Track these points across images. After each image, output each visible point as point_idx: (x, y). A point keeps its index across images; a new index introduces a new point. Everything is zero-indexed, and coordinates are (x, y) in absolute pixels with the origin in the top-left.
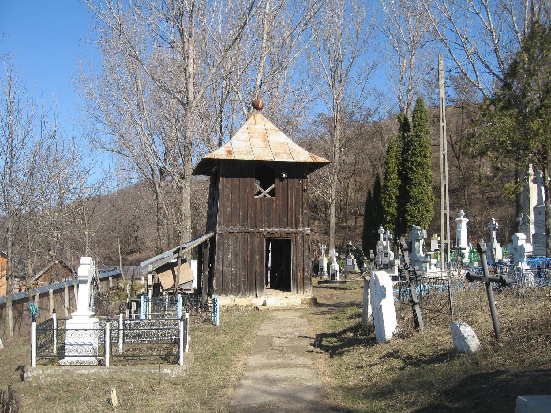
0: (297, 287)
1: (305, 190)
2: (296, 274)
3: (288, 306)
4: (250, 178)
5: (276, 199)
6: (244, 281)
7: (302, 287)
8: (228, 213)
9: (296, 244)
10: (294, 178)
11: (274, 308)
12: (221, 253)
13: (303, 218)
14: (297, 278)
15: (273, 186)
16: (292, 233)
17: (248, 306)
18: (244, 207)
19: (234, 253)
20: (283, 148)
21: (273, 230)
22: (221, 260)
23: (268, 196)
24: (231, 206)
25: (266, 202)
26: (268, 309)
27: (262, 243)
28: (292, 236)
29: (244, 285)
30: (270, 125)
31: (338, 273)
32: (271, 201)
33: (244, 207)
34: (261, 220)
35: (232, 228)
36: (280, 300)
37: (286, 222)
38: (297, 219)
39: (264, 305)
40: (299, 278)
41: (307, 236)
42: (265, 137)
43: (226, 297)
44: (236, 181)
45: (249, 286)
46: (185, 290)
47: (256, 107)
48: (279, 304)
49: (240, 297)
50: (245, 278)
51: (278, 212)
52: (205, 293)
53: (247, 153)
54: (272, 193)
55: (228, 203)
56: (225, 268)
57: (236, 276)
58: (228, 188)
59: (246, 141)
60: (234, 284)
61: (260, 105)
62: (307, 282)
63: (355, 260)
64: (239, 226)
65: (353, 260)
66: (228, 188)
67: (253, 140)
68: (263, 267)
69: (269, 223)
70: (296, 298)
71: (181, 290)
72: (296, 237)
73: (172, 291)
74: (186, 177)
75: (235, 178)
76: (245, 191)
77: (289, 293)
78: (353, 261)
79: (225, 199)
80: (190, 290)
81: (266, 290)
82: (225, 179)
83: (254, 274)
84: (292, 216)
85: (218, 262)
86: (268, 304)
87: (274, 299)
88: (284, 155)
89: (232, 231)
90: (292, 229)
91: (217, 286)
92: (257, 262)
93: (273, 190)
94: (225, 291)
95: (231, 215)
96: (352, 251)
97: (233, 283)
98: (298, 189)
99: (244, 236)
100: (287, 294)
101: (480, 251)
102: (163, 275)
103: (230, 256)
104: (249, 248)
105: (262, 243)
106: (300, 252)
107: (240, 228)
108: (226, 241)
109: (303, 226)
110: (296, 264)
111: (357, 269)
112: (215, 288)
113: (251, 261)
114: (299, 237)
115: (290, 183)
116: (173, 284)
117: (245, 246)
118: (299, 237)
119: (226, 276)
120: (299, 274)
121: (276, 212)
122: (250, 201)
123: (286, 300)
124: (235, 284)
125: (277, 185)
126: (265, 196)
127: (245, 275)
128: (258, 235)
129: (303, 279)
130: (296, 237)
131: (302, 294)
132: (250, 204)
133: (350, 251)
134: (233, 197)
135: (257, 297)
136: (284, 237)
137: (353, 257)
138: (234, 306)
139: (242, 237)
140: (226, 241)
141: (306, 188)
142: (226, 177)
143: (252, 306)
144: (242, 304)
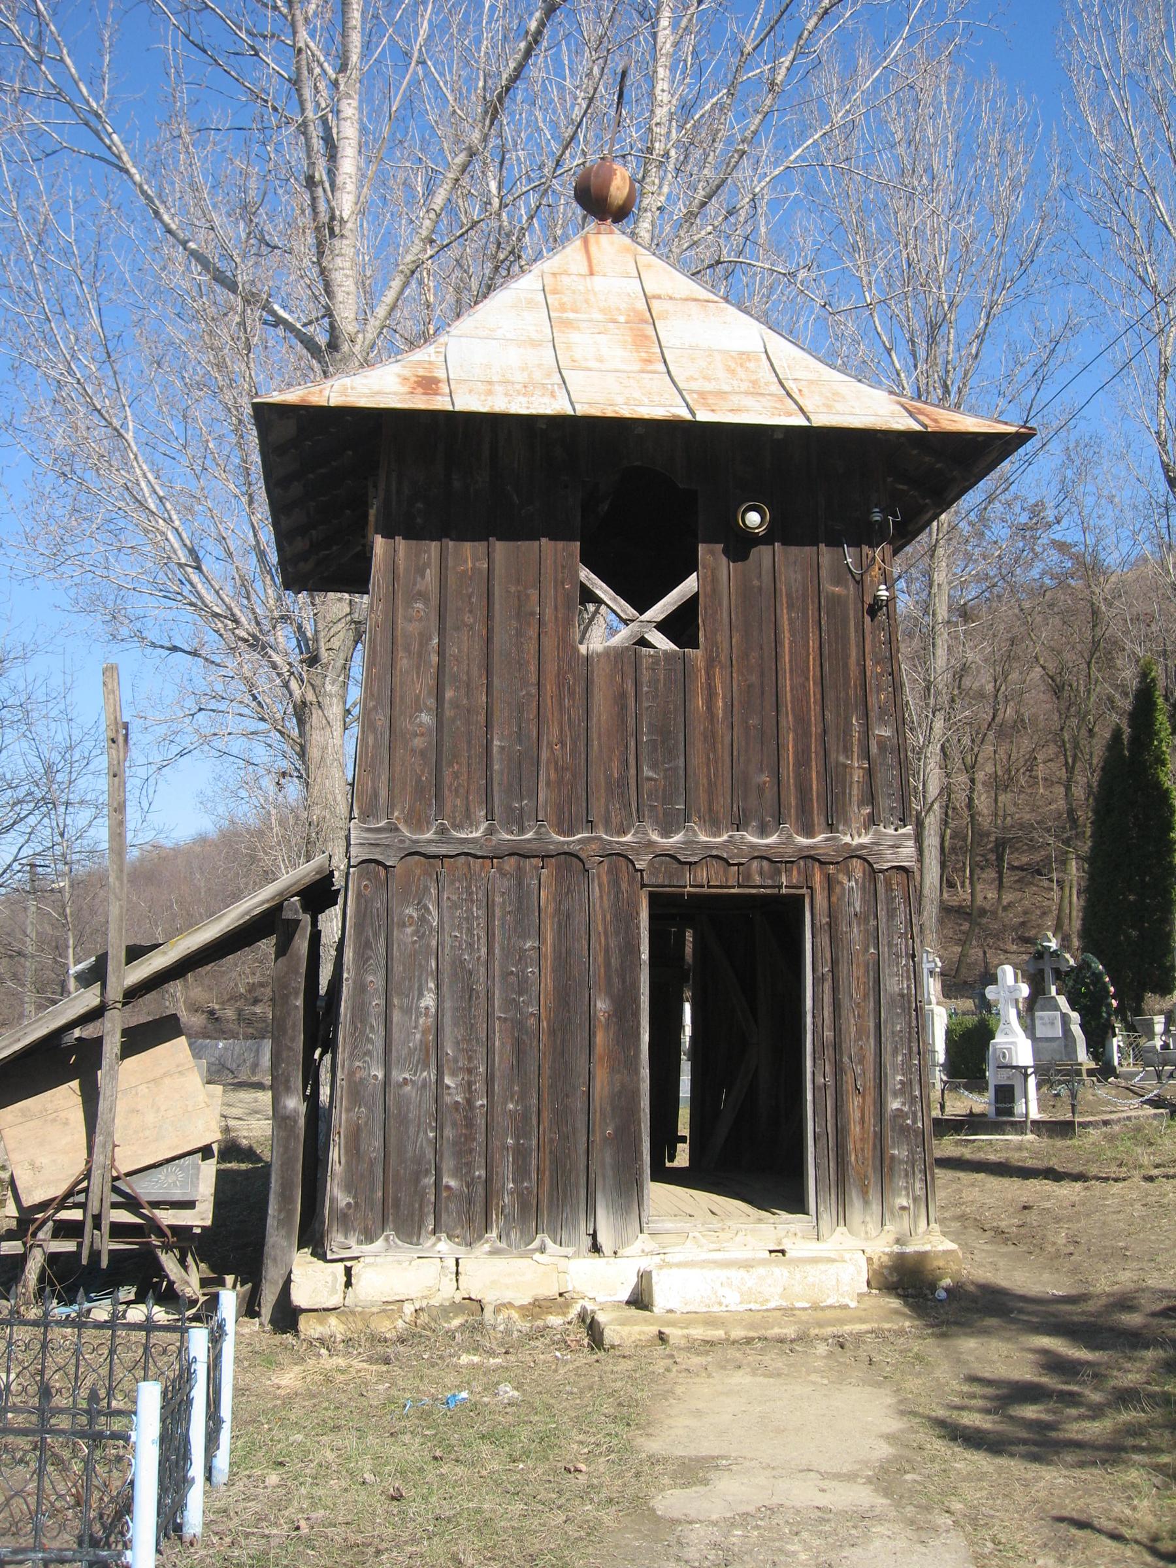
0: (840, 1185)
1: (874, 608)
2: (839, 1108)
3: (788, 1311)
4: (554, 537)
5: (710, 663)
6: (521, 1153)
7: (873, 1179)
8: (418, 743)
9: (832, 925)
10: (814, 543)
11: (698, 1332)
12: (375, 980)
13: (870, 772)
14: (841, 1132)
15: (690, 585)
16: (810, 858)
17: (538, 1307)
18: (520, 708)
19: (464, 988)
20: (741, 373)
21: (689, 844)
22: (377, 1023)
23: (662, 642)
24: (440, 698)
25: (646, 676)
26: (662, 1337)
27: (624, 919)
28: (808, 877)
29: (521, 1173)
30: (667, 280)
31: (1032, 1081)
32: (681, 672)
33: (520, 708)
34: (622, 783)
35: (442, 830)
36: (736, 1274)
37: (770, 795)
38: (834, 778)
39: (640, 1300)
40: (855, 1130)
41: (897, 879)
42: (644, 325)
43: (406, 1252)
44: (468, 556)
45: (550, 1189)
46: (156, 1205)
47: (597, 204)
48: (733, 1301)
49: (494, 1252)
50: (521, 1132)
51: (721, 729)
52: (285, 1223)
53: (526, 388)
54: (680, 626)
55: (421, 686)
56: (398, 1076)
57: (469, 1123)
58: (422, 596)
59: (534, 344)
60: (456, 1174)
61: (619, 189)
62: (899, 1152)
63: (1075, 1016)
64: (490, 816)
65: (1064, 1016)
66: (422, 596)
67: (574, 337)
68: (632, 1065)
69: (667, 799)
70: (828, 1259)
71: (131, 1203)
72: (830, 882)
73: (76, 1215)
74: (324, 655)
75: (461, 538)
76: (521, 614)
77: (796, 1222)
78: (1065, 1019)
79: (404, 663)
80: (190, 1205)
81: (659, 1193)
82: (401, 544)
83: (579, 1104)
84: (803, 761)
85: (359, 1036)
86: (662, 1299)
87: (703, 1258)
88: (749, 402)
89: (443, 850)
90: (809, 833)
91: (349, 1186)
92: (600, 1038)
93: (690, 607)
94: (401, 1211)
95: (439, 753)
96: (1058, 975)
97: (448, 1164)
98: (837, 602)
99: (520, 873)
100: (782, 1227)
101: (356, 1028)
102: (27, 1115)
103: (429, 1000)
104: (548, 949)
105: (624, 919)
106: (855, 975)
107: (490, 831)
108: (410, 911)
109: (872, 821)
110: (837, 1046)
111: (1082, 1055)
112: (337, 1194)
113: (561, 1030)
114: (852, 883)
115: (784, 564)
116: (81, 1167)
117: (524, 936)
118: (852, 883)
119: (403, 1120)
120: (853, 1105)
121: (711, 738)
122: (551, 668)
123: (779, 1273)
124: (463, 1170)
125: (715, 580)
126: (643, 642)
127: (525, 1116)
128: (601, 872)
129: (880, 1137)
130: (830, 882)
131: (872, 1227)
132: (550, 688)
133: (1049, 975)
134: (452, 650)
135: (596, 1248)
136: (759, 881)
137: (1062, 1001)
138: (455, 1308)
139: (504, 884)
140: (410, 911)
141: (883, 593)
142: (413, 533)
143: (567, 1305)
144: (508, 1296)
